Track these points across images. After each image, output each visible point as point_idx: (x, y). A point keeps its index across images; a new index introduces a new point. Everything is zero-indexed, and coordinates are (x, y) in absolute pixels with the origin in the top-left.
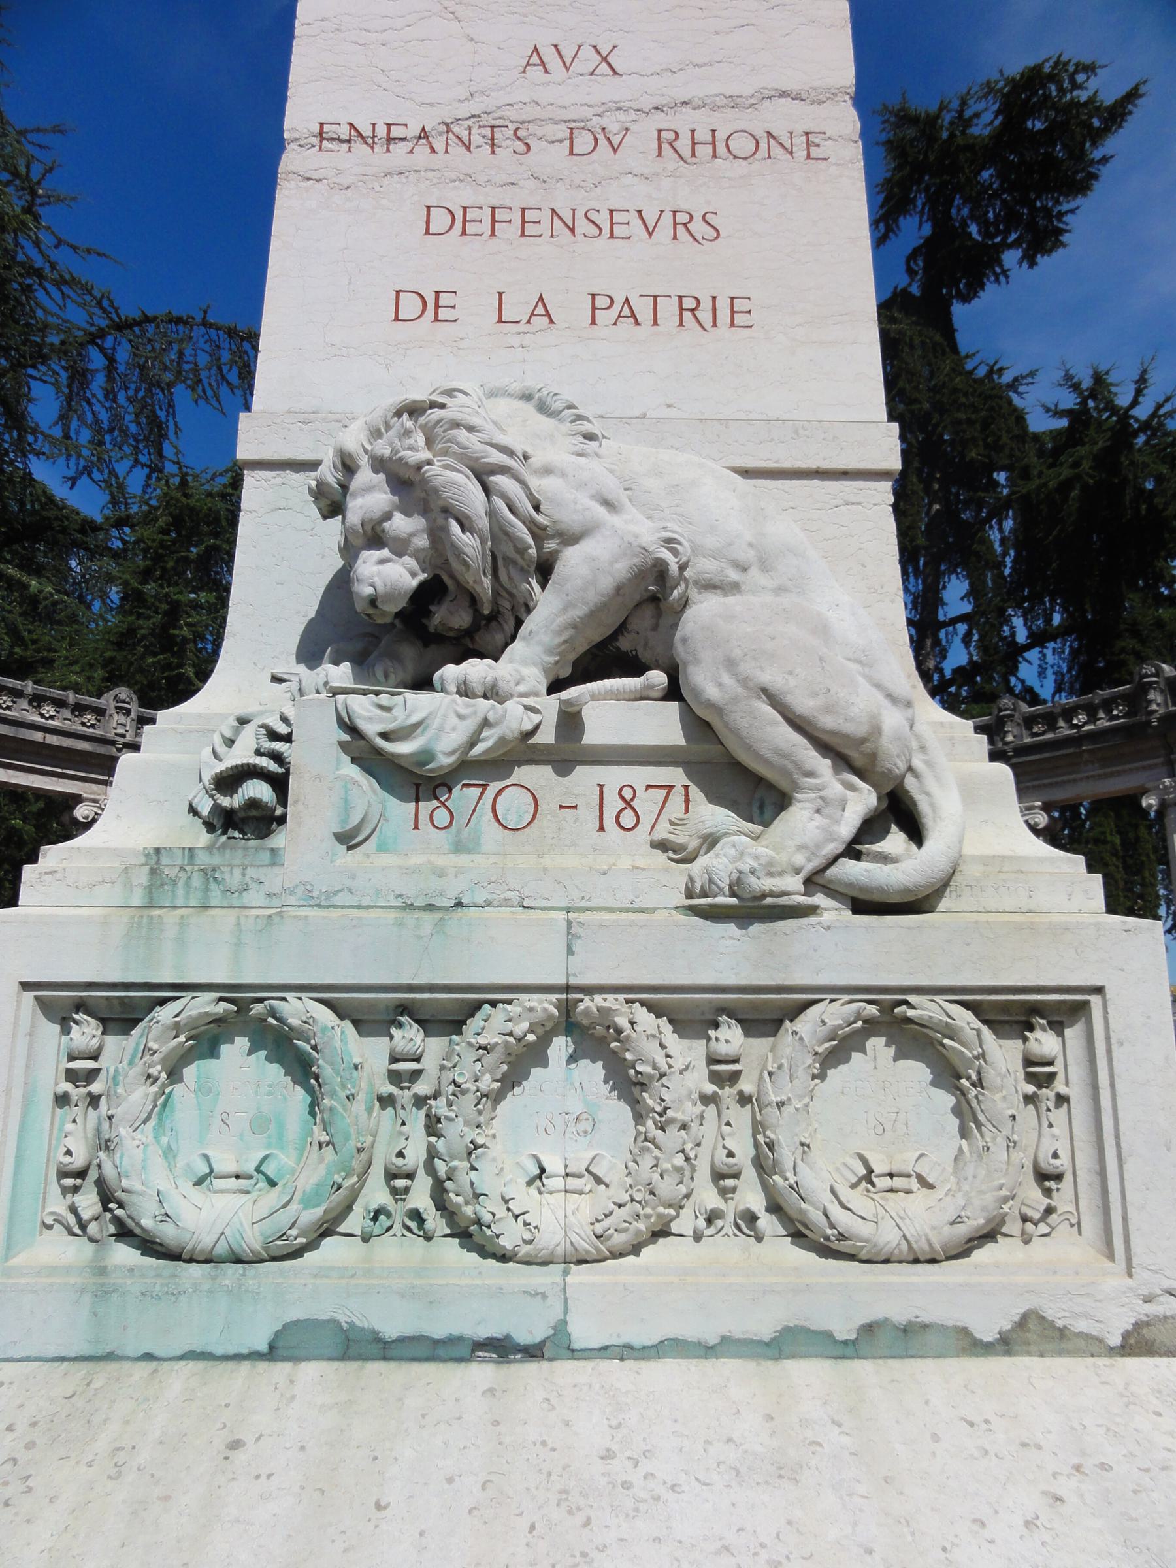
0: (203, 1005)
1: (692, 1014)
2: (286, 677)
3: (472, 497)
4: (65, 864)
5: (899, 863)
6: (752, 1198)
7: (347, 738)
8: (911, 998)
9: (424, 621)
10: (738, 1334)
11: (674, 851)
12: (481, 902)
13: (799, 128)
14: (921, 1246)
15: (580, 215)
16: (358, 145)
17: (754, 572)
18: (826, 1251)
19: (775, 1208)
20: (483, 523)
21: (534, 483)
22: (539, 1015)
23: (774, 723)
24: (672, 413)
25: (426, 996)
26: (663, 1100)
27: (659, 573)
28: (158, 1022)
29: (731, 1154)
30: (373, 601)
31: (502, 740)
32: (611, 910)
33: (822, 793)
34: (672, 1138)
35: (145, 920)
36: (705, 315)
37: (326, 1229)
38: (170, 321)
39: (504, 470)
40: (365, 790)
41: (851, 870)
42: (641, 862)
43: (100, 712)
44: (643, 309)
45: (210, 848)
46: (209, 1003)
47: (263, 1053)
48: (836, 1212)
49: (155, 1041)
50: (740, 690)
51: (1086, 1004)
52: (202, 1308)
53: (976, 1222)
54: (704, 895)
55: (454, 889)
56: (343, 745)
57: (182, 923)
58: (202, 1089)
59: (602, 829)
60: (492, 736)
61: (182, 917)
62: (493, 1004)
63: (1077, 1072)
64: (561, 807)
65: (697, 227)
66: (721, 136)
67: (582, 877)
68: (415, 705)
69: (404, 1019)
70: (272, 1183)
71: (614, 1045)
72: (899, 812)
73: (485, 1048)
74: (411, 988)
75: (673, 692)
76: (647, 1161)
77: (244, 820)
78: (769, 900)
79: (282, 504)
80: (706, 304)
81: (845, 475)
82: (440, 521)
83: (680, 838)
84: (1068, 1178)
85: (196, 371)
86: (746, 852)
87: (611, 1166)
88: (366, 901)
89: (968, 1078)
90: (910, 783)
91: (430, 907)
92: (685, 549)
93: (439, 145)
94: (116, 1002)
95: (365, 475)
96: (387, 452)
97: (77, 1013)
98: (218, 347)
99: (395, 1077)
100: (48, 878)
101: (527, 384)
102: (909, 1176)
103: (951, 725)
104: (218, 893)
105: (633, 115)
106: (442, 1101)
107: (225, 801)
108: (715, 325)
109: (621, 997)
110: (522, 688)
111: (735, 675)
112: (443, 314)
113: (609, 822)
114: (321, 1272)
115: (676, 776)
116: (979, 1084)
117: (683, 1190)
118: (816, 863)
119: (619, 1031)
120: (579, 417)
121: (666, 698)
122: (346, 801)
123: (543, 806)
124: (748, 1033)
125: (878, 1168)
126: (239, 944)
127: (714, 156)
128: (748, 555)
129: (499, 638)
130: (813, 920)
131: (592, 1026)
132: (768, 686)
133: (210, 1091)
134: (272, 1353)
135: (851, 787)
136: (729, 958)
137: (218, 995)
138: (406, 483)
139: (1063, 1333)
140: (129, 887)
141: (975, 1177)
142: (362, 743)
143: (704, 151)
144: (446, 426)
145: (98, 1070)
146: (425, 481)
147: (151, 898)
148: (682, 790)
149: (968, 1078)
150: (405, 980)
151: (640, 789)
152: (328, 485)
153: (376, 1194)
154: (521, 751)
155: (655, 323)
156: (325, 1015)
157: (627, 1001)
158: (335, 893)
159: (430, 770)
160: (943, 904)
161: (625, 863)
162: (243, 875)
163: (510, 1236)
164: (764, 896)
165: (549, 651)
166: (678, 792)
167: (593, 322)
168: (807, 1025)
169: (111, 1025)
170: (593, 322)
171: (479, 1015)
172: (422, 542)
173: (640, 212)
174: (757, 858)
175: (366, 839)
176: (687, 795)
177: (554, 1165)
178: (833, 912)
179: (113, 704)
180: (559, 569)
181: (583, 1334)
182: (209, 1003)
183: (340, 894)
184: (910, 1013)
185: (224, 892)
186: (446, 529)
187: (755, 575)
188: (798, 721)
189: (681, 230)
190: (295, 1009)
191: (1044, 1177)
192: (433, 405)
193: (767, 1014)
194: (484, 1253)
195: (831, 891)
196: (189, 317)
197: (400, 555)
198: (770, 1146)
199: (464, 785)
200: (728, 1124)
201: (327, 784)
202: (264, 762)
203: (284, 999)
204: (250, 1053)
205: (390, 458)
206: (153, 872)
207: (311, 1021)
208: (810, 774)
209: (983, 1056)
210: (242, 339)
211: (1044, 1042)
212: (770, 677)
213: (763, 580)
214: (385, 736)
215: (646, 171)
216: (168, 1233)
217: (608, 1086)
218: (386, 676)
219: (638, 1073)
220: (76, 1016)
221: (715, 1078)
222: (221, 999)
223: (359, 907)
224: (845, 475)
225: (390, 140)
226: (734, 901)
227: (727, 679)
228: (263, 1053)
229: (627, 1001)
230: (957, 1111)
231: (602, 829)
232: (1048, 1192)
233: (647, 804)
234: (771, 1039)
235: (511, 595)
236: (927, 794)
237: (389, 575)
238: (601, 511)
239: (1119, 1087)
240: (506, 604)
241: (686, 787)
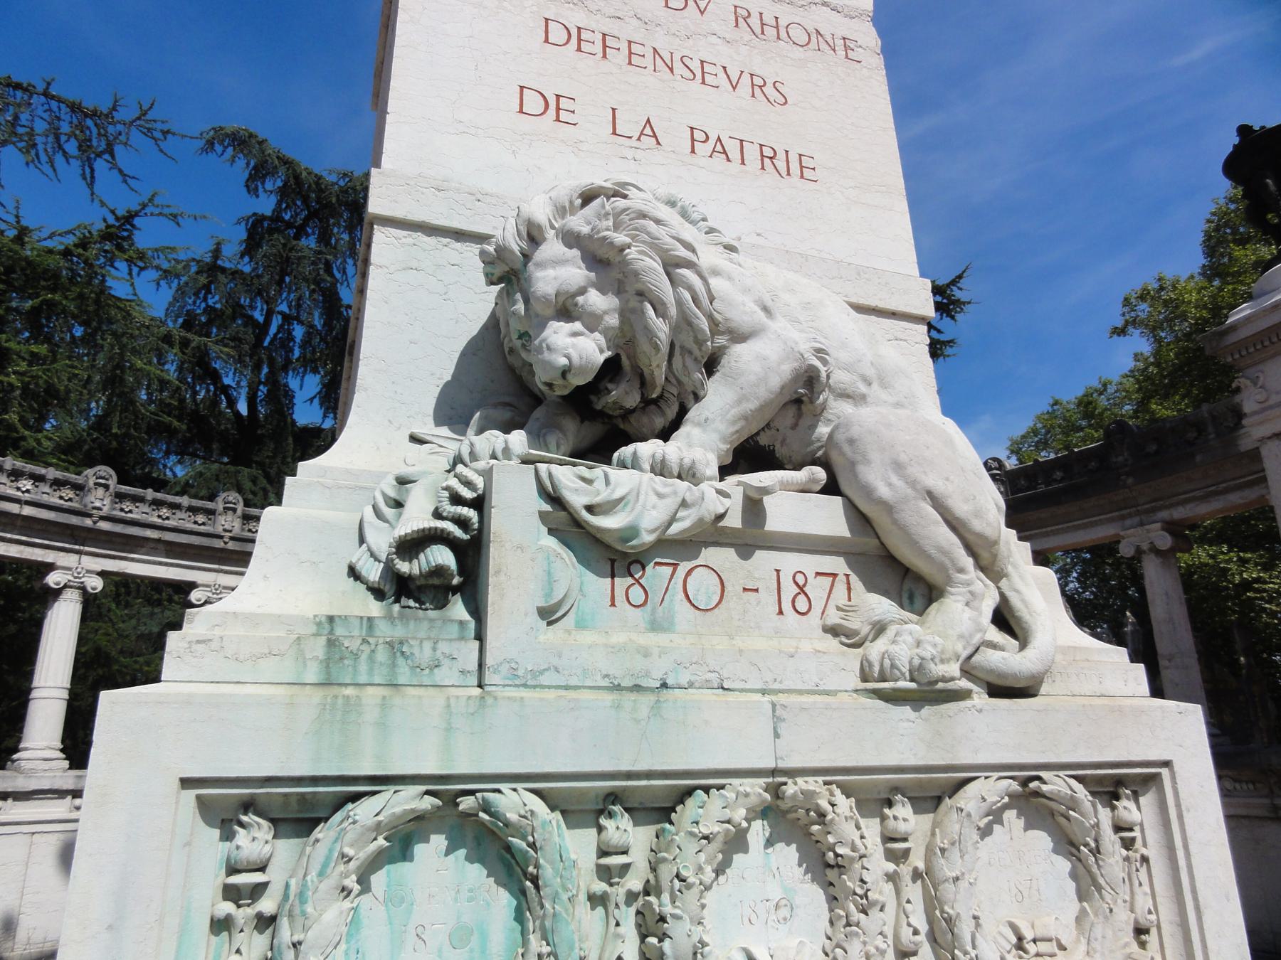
0: (409, 800)
1: (876, 794)
2: (429, 438)
4: (218, 632)
7: (548, 508)
8: (1043, 774)
9: (593, 398)
11: (847, 637)
12: (684, 682)
13: (839, 34)
15: (677, 58)
17: (875, 386)
20: (673, 311)
21: (713, 282)
22: (753, 800)
23: (936, 523)
24: (760, 241)
25: (643, 783)
26: (865, 883)
28: (354, 822)
31: (701, 521)
32: (800, 692)
33: (971, 588)
35: (340, 701)
38: (8, 85)
39: (690, 265)
42: (820, 646)
46: (413, 798)
47: (462, 852)
49: (351, 846)
50: (909, 491)
51: (1159, 774)
54: (883, 679)
55: (658, 670)
56: (543, 516)
57: (384, 704)
58: (394, 900)
59: (781, 612)
60: (689, 516)
61: (384, 698)
62: (706, 789)
64: (745, 589)
65: (769, 90)
66: (783, 23)
69: (617, 808)
71: (816, 828)
73: (706, 838)
74: (629, 775)
75: (831, 488)
77: (420, 588)
78: (940, 685)
79: (414, 265)
81: (893, 315)
82: (633, 303)
83: (854, 623)
84: (1154, 931)
85: (31, 134)
86: (913, 640)
88: (574, 681)
89: (1086, 845)
91: (637, 688)
94: (293, 800)
95: (552, 247)
96: (585, 230)
97: (246, 813)
98: (59, 119)
99: (605, 873)
100: (201, 647)
101: (673, 192)
102: (1050, 940)
104: (407, 669)
107: (404, 567)
108: (789, 174)
109: (820, 779)
112: (564, 116)
113: (787, 606)
115: (837, 564)
119: (822, 815)
121: (824, 491)
122: (549, 573)
123: (728, 588)
124: (917, 811)
125: (1029, 935)
126: (449, 729)
127: (778, 38)
128: (871, 373)
130: (967, 703)
131: (793, 809)
132: (933, 489)
133: (402, 901)
136: (904, 740)
137: (424, 788)
138: (603, 261)
140: (301, 659)
141: (1104, 937)
142: (563, 514)
143: (771, 32)
144: (632, 215)
145: (265, 885)
146: (625, 263)
147: (328, 673)
148: (844, 578)
149: (1086, 845)
150: (625, 767)
151: (811, 576)
152: (512, 252)
154: (710, 534)
155: (743, 163)
157: (826, 783)
158: (542, 673)
159: (633, 547)
161: (806, 646)
162: (434, 649)
164: (936, 682)
165: (724, 440)
166: (841, 578)
167: (693, 151)
169: (283, 827)
170: (693, 151)
171: (690, 802)
172: (613, 320)
173: (724, 68)
174: (935, 645)
175: (564, 615)
176: (848, 583)
178: (980, 698)
182: (413, 798)
183: (547, 674)
184: (1045, 788)
185: (413, 668)
188: (954, 522)
189: (757, 90)
190: (513, 803)
193: (934, 791)
196: (29, 85)
197: (592, 331)
199: (657, 564)
200: (908, 902)
201: (523, 556)
203: (499, 791)
204: (447, 853)
205: (590, 236)
206: (332, 643)
207: (529, 815)
208: (961, 571)
210: (86, 115)
212: (932, 481)
213: (884, 395)
214: (590, 509)
215: (727, 36)
217: (802, 870)
218: (558, 447)
219: (837, 855)
220: (244, 818)
222: (428, 793)
223: (567, 688)
224: (893, 315)
226: (913, 685)
227: (894, 479)
228: (462, 852)
229: (826, 783)
230: (1074, 875)
231: (781, 612)
233: (817, 588)
234: (932, 815)
235: (679, 382)
236: (1017, 591)
237: (574, 348)
239: (1192, 848)
241: (847, 576)
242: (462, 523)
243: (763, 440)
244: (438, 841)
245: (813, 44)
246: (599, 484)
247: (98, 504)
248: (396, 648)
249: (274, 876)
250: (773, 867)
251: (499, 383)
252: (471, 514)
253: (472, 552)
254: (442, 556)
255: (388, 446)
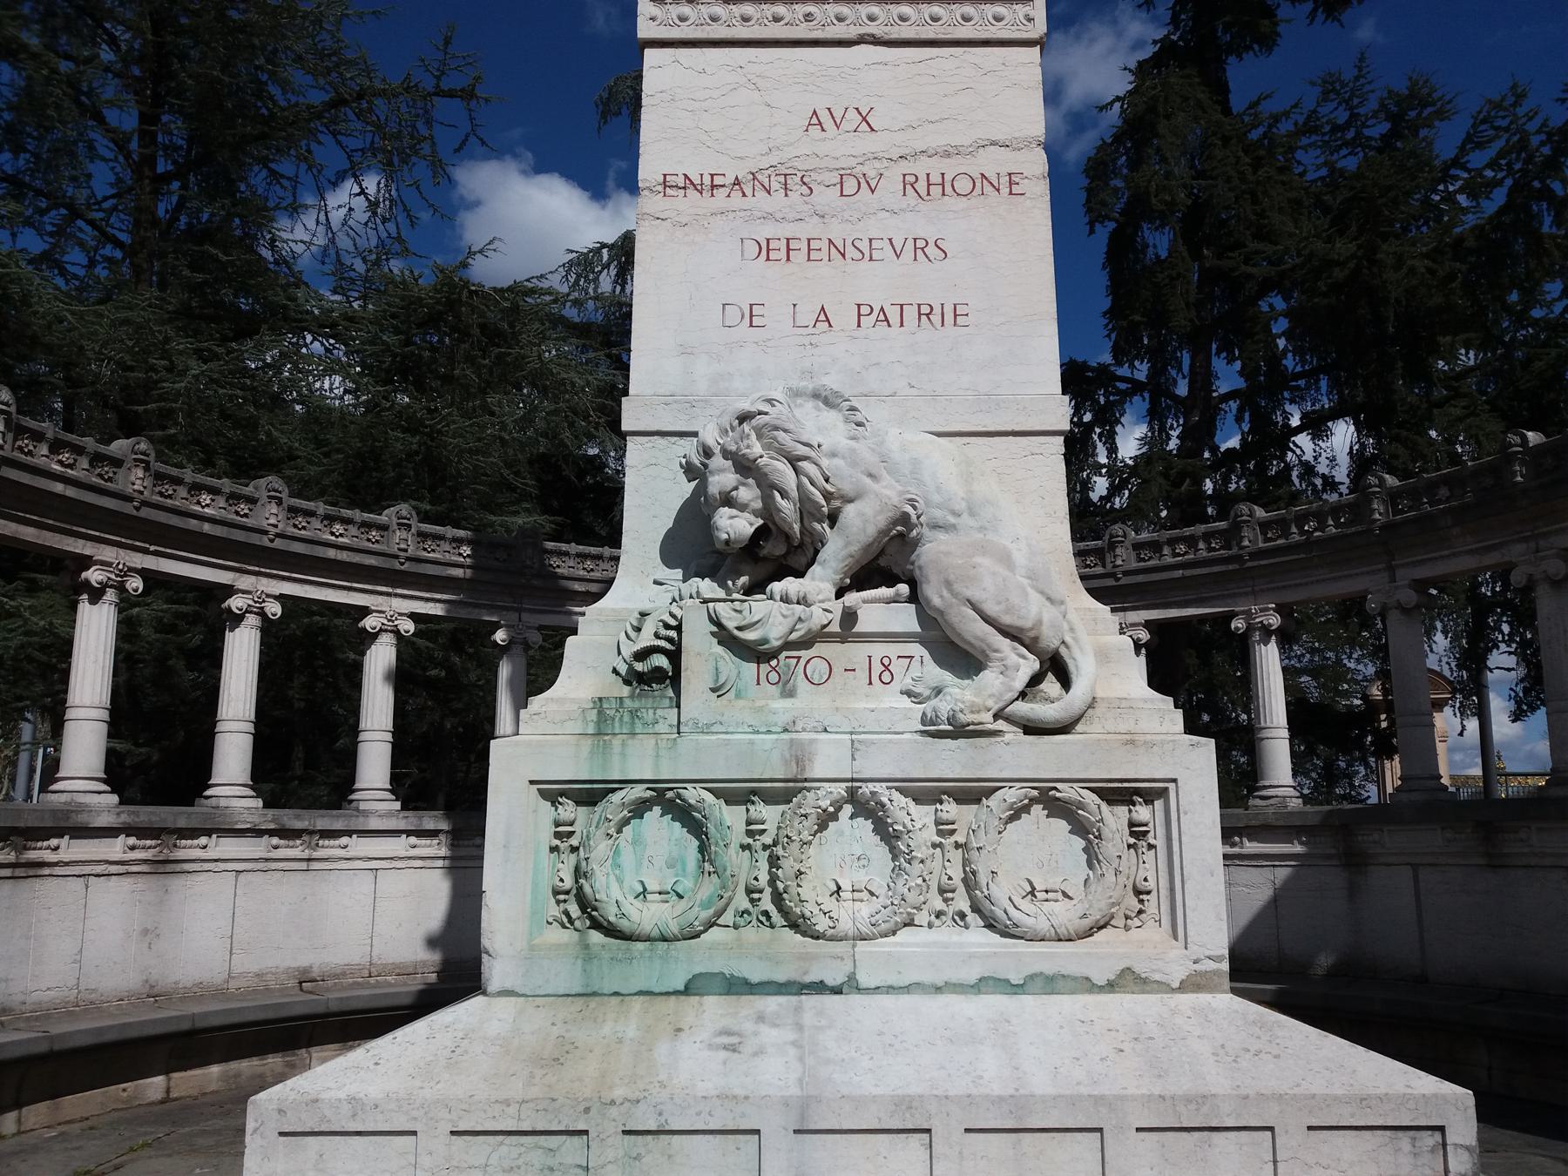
0: (639, 792)
1: (926, 793)
3: (784, 474)
5: (1052, 704)
6: (963, 904)
8: (1058, 785)
10: (954, 980)
13: (1004, 171)
14: (1062, 931)
15: (848, 243)
16: (691, 192)
17: (965, 516)
18: (1005, 934)
19: (976, 909)
20: (794, 494)
21: (825, 462)
22: (835, 796)
27: (904, 519)
29: (950, 878)
30: (727, 542)
34: (917, 868)
36: (936, 318)
37: (710, 924)
40: (729, 664)
41: (1022, 708)
43: (252, 501)
44: (894, 317)
45: (632, 696)
48: (1011, 910)
52: (645, 967)
53: (1096, 916)
57: (623, 744)
58: (636, 842)
63: (1161, 831)
66: (948, 178)
67: (864, 710)
68: (759, 606)
69: (755, 799)
70: (680, 897)
72: (1056, 667)
75: (914, 598)
76: (900, 882)
80: (937, 310)
84: (1154, 893)
87: (879, 885)
90: (1063, 651)
92: (921, 505)
93: (748, 192)
95: (717, 461)
103: (1096, 610)
105: (885, 163)
106: (779, 848)
107: (639, 667)
110: (821, 597)
111: (951, 591)
112: (756, 321)
114: (713, 947)
115: (917, 650)
116: (1099, 837)
117: (922, 899)
118: (1001, 705)
119: (883, 806)
120: (852, 409)
126: (657, 756)
128: (960, 506)
129: (804, 561)
131: (868, 802)
134: (687, 991)
135: (1024, 657)
138: (745, 467)
139: (1145, 981)
143: (935, 190)
151: (894, 659)
153: (742, 902)
156: (709, 798)
160: (1079, 728)
163: (822, 924)
165: (836, 572)
168: (993, 802)
172: (758, 505)
177: (846, 885)
178: (1013, 734)
179: (395, 520)
180: (842, 519)
181: (864, 980)
186: (773, 498)
187: (966, 520)
190: (692, 794)
191: (1138, 892)
192: (760, 413)
193: (971, 794)
194: (804, 934)
195: (1009, 720)
198: (974, 873)
201: (700, 648)
202: (663, 643)
206: (601, 712)
209: (1102, 820)
211: (1142, 813)
213: (971, 522)
214: (739, 628)
216: (624, 924)
221: (940, 833)
225: (713, 187)
227: (945, 593)
232: (1141, 902)
233: (898, 667)
237: (735, 525)
238: (868, 481)
240: (807, 540)
242: (669, 640)
243: (882, 562)
244: (657, 810)
245: (978, 190)
246: (746, 613)
247: (272, 521)
248: (634, 713)
249: (577, 828)
250: (854, 833)
251: (692, 547)
252: (673, 634)
253: (675, 656)
254: (661, 661)
255: (640, 588)
